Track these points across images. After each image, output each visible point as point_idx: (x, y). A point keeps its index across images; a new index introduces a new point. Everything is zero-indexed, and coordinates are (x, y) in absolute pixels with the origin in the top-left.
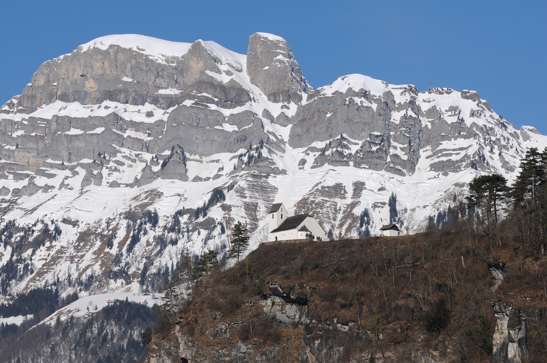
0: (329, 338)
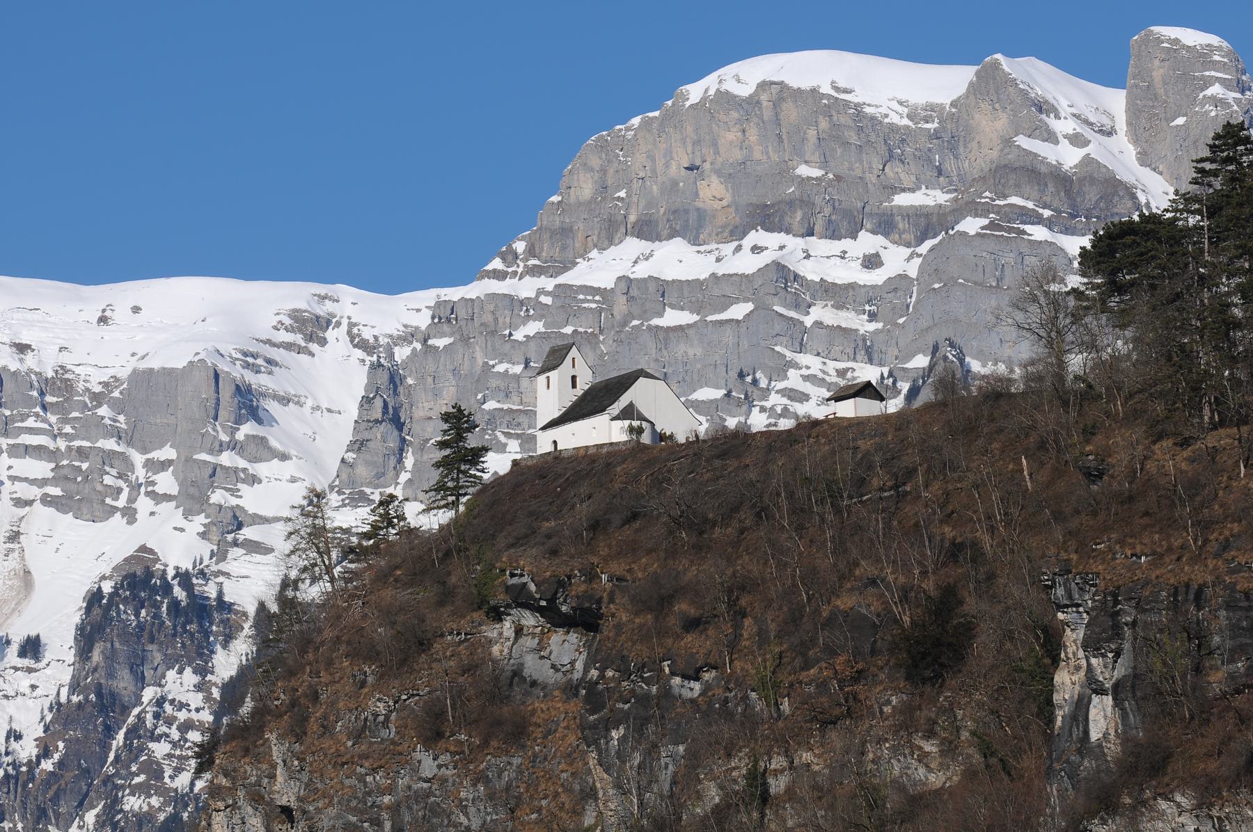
0: (647, 720)
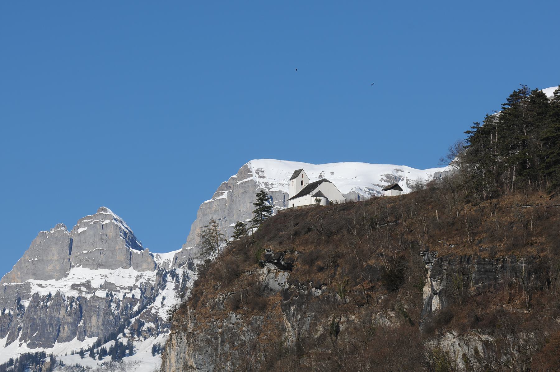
0: (303, 303)
